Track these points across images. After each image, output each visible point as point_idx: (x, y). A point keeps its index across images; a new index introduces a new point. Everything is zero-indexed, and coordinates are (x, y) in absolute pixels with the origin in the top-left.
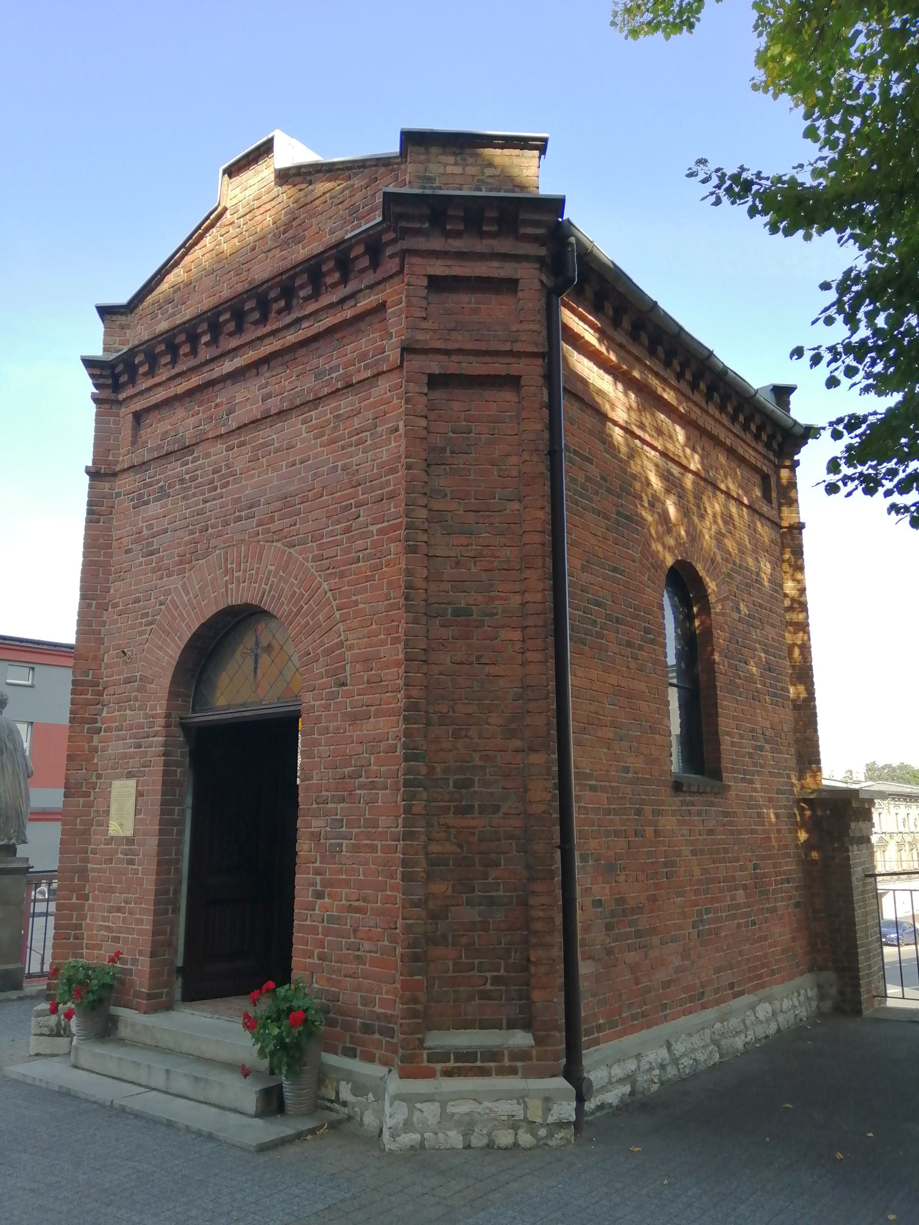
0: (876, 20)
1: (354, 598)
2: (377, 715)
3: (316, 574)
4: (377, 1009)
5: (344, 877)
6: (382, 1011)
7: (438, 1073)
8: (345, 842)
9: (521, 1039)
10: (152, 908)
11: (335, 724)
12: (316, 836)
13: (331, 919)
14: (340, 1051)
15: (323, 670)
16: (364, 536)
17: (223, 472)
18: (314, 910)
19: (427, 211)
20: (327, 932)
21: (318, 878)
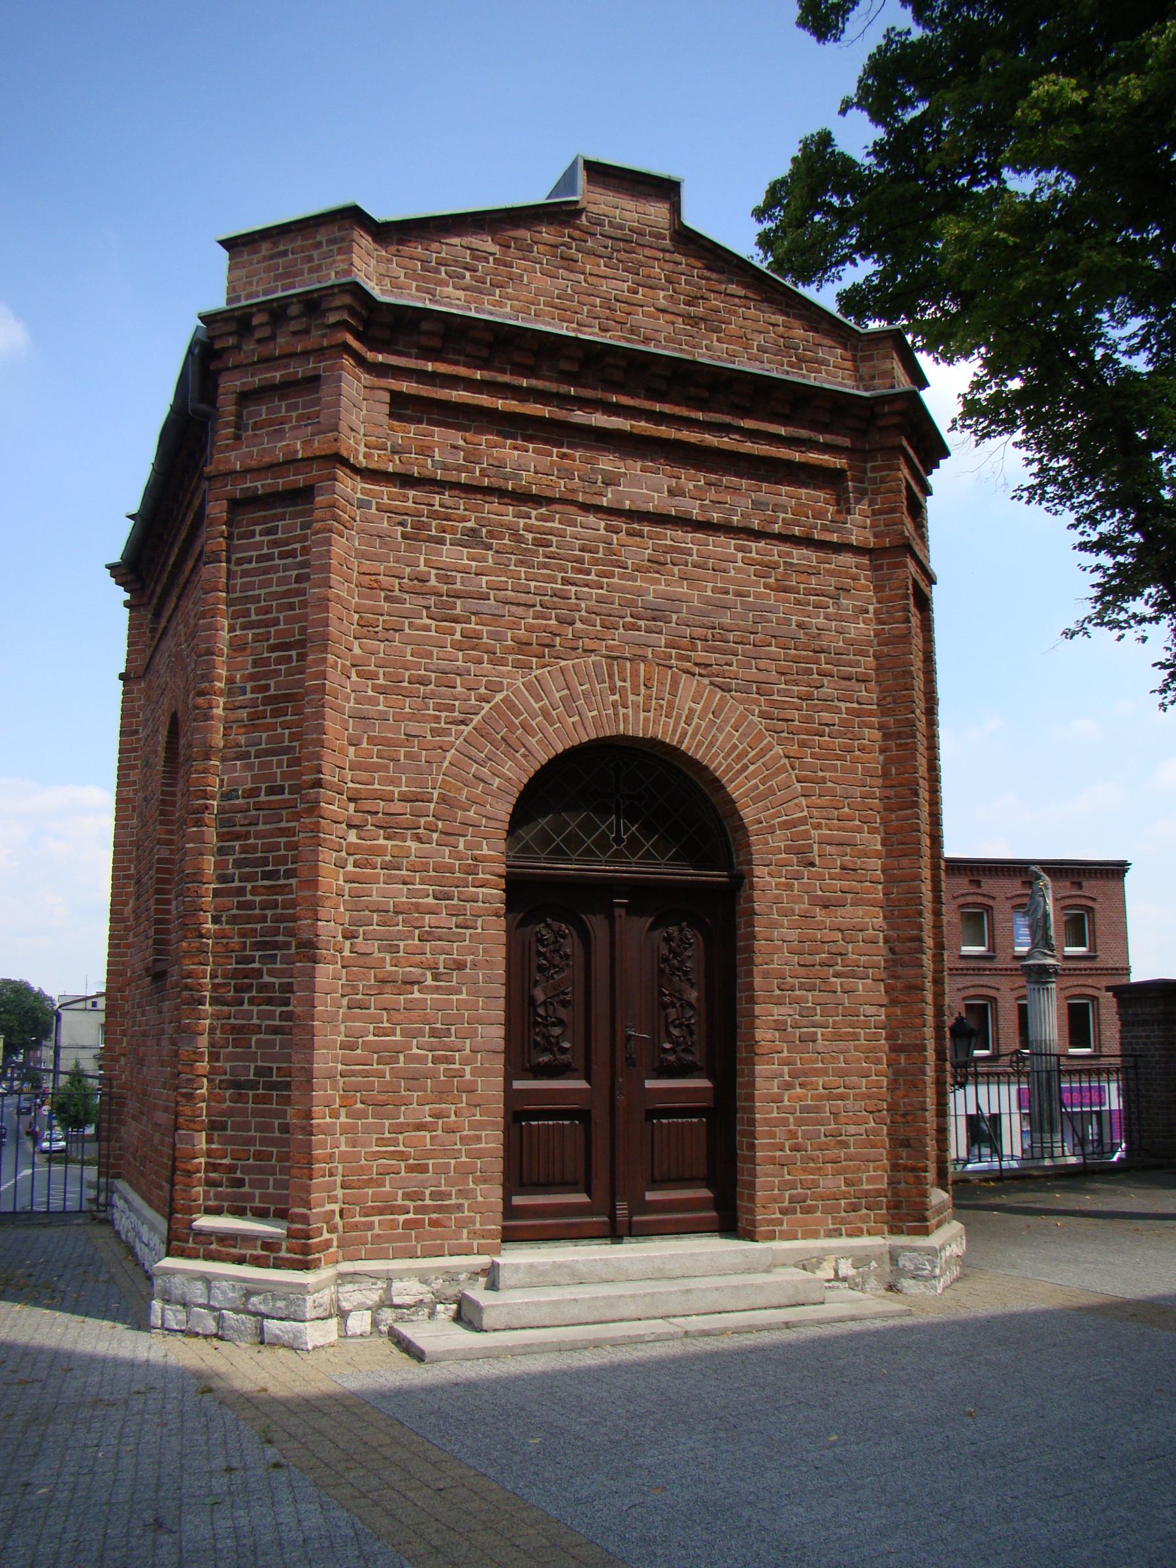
0: (1104, 479)
1: (820, 774)
2: (853, 904)
3: (767, 734)
4: (865, 1187)
5: (820, 1065)
6: (871, 1187)
7: (822, 1233)
8: (819, 1031)
9: (582, 1198)
10: (758, 1116)
11: (802, 906)
12: (780, 1027)
13: (805, 1109)
14: (799, 1235)
15: (782, 844)
16: (830, 709)
17: (280, 535)
18: (782, 1101)
19: (624, 364)
20: (799, 1122)
21: (786, 1069)
